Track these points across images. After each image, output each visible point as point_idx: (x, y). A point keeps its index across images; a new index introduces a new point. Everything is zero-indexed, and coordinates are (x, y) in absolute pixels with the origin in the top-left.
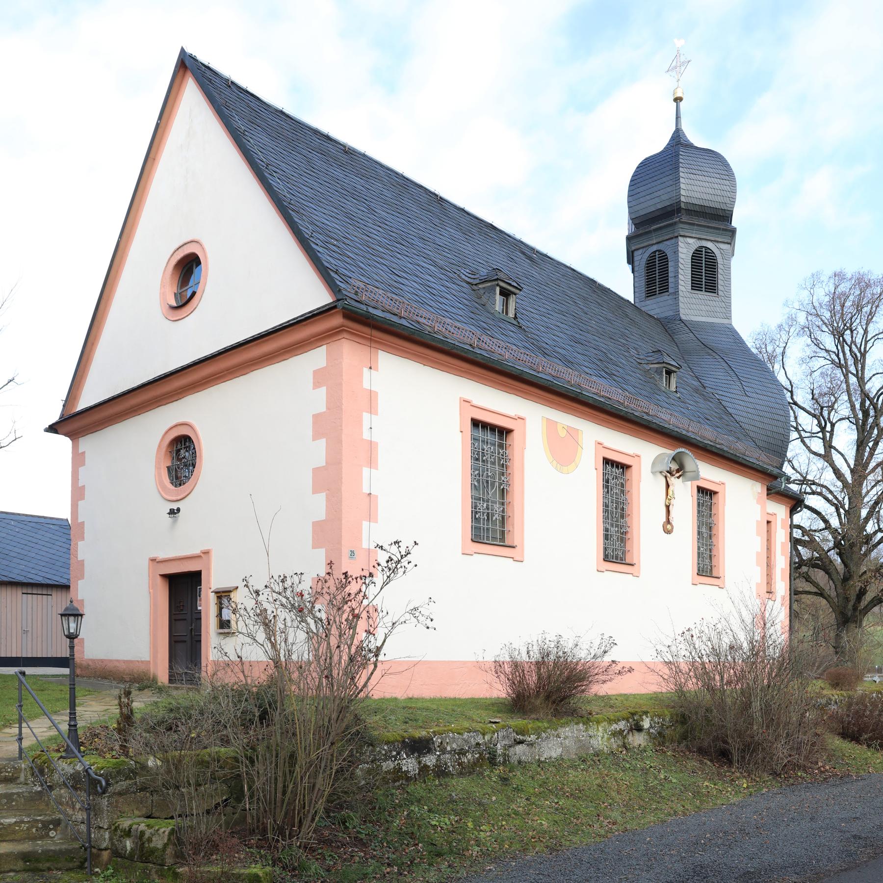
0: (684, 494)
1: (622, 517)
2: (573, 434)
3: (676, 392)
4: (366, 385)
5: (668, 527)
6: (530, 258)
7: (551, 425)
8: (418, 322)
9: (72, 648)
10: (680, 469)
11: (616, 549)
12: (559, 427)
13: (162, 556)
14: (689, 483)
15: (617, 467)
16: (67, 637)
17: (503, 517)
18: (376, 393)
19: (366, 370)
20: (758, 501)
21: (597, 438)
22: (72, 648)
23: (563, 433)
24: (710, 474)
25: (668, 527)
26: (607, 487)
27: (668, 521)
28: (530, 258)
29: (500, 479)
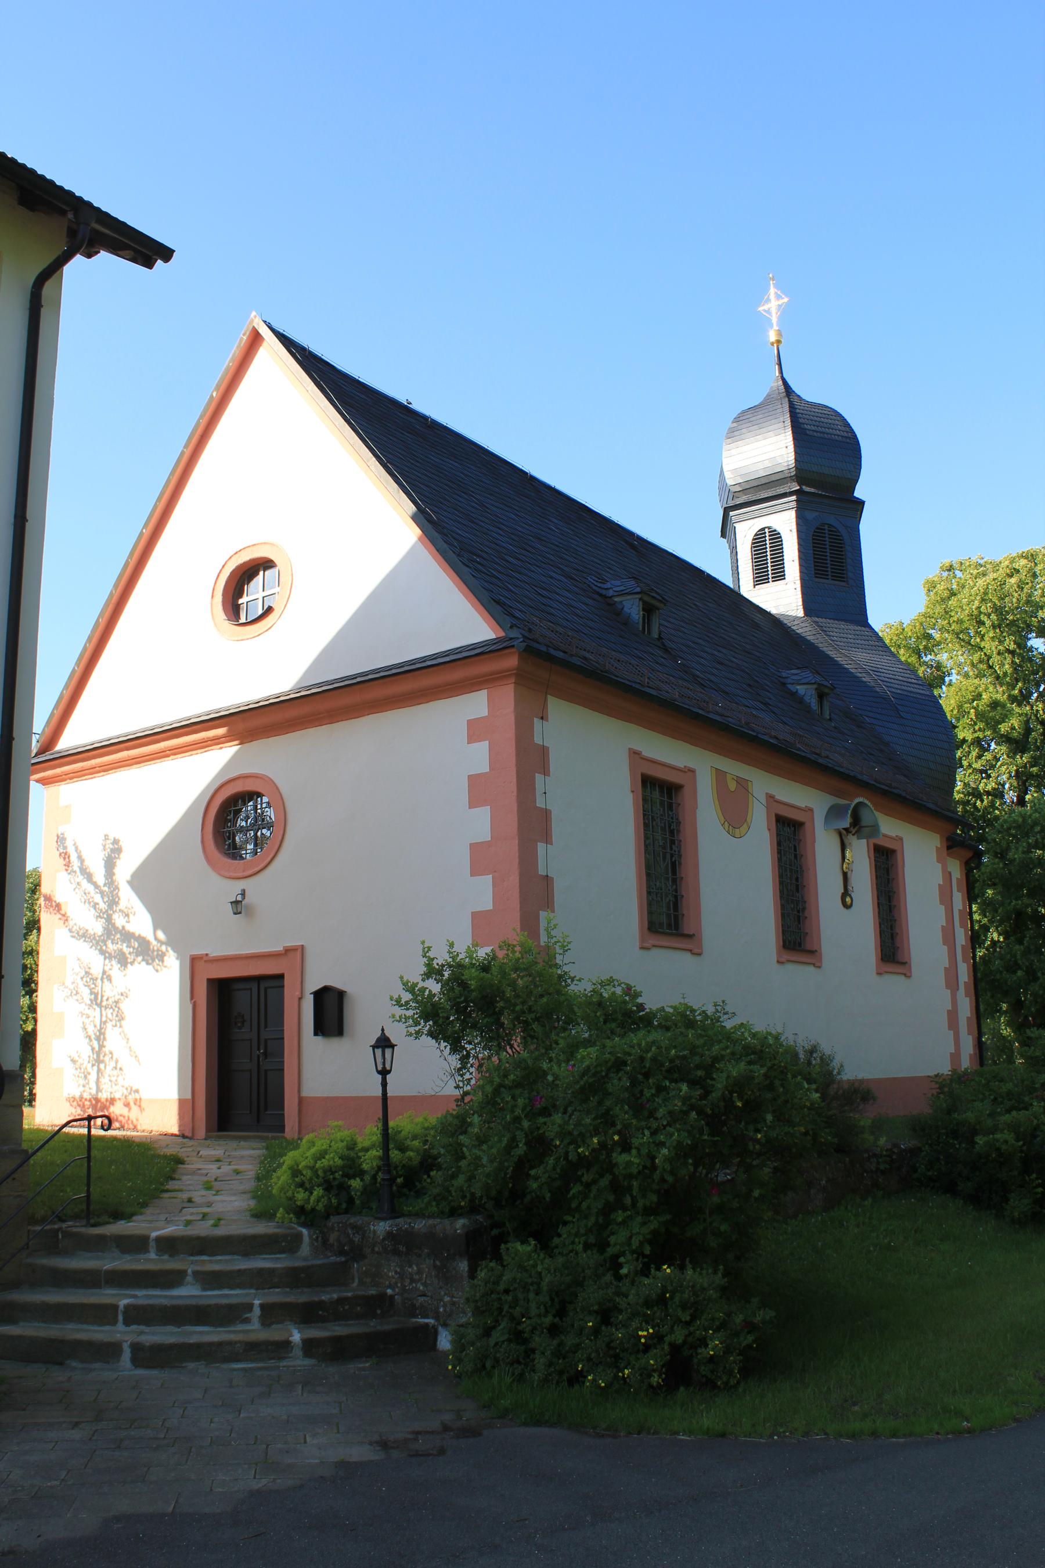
0: (860, 853)
1: (797, 890)
2: (743, 784)
3: (830, 719)
4: (537, 740)
5: (846, 899)
6: (633, 547)
7: (720, 776)
8: (585, 659)
9: (384, 1084)
10: (857, 825)
11: (796, 936)
12: (729, 777)
13: (811, 968)
14: (865, 841)
15: (789, 825)
16: (379, 1072)
17: (676, 897)
18: (548, 748)
19: (537, 722)
20: (939, 860)
21: (770, 789)
22: (384, 1084)
23: (732, 786)
24: (889, 827)
25: (846, 899)
26: (672, 832)
27: (846, 893)
28: (633, 547)
29: (671, 849)
